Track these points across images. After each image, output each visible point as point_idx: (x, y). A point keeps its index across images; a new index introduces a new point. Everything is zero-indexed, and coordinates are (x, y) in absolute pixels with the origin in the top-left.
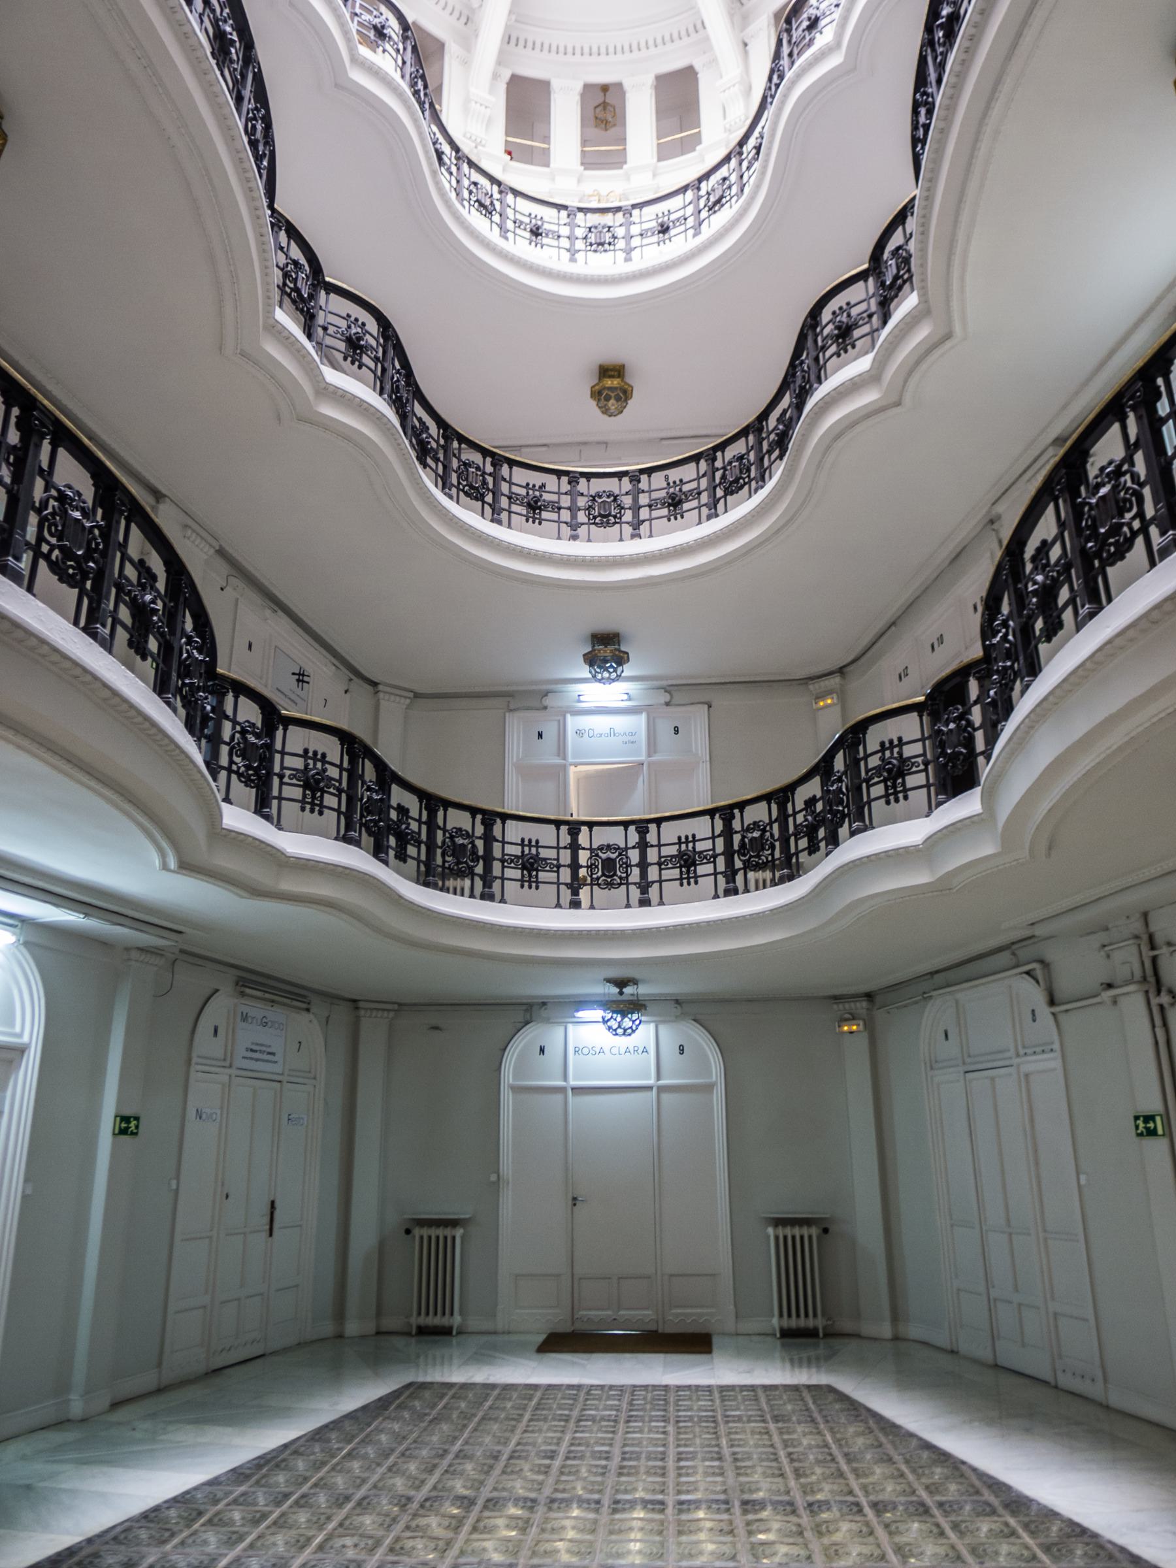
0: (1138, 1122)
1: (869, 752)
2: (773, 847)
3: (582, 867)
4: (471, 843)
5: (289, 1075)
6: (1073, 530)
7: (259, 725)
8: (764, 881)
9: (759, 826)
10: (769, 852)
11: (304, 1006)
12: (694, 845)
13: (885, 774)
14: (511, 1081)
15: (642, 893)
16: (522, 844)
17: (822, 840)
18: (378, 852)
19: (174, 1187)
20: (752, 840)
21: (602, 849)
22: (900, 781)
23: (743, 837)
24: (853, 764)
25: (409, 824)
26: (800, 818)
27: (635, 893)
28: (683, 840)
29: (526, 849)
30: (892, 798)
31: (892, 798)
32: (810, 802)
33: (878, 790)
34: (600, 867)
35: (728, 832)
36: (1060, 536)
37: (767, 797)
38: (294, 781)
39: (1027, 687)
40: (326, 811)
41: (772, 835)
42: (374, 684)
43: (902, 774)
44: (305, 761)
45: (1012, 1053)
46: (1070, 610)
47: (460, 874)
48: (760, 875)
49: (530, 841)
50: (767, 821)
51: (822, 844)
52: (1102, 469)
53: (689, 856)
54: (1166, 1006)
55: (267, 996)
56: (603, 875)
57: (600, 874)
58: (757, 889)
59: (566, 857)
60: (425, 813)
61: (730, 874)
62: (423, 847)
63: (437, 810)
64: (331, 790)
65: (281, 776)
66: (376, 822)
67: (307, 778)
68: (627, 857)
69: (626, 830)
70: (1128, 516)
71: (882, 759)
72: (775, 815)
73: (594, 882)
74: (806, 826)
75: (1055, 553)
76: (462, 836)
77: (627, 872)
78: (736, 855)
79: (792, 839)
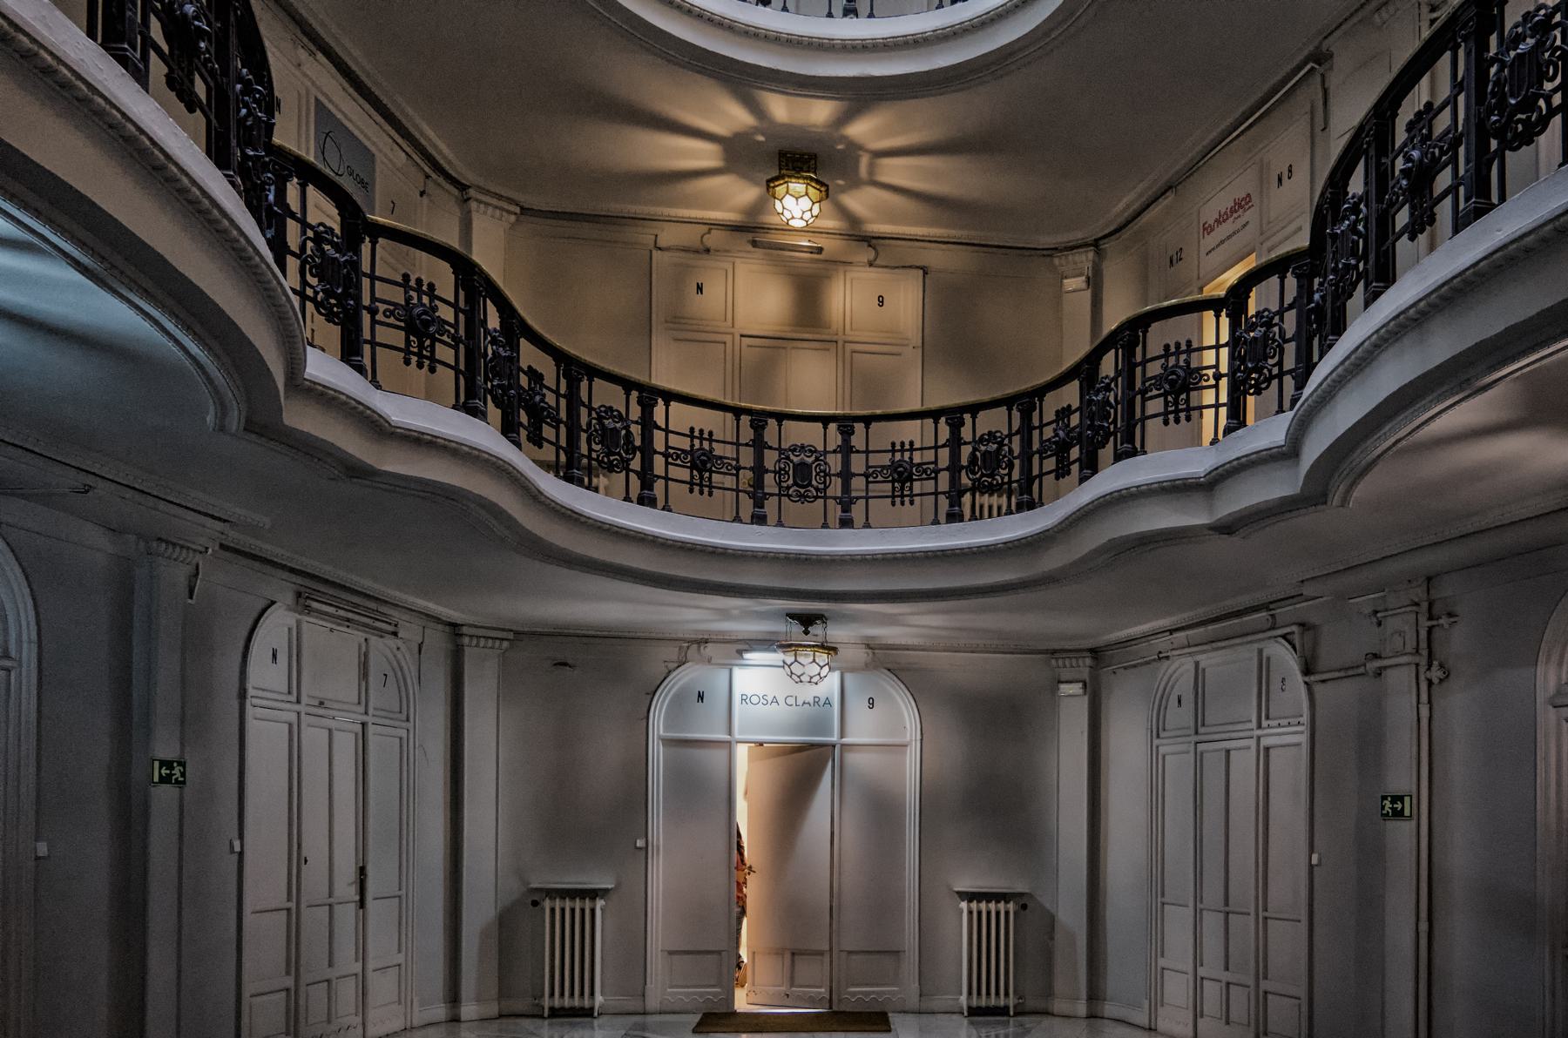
0: (1385, 802)
1: (1149, 356)
2: (1011, 466)
3: (767, 471)
4: (624, 428)
5: (374, 716)
6: (1473, 92)
7: (338, 231)
8: (999, 508)
9: (995, 438)
10: (1006, 471)
11: (391, 628)
12: (912, 454)
13: (1167, 387)
14: (661, 732)
15: (844, 511)
16: (691, 436)
17: (1074, 462)
18: (509, 429)
19: (237, 849)
20: (984, 454)
21: (795, 450)
22: (1183, 396)
23: (975, 449)
24: (1127, 370)
25: (544, 395)
26: (1048, 432)
27: (835, 511)
28: (898, 447)
29: (697, 442)
30: (1171, 417)
31: (1171, 417)
32: (1064, 413)
33: (1155, 406)
34: (791, 472)
35: (955, 442)
36: (1452, 101)
37: (1007, 402)
38: (392, 320)
39: (1376, 295)
40: (439, 368)
41: (1011, 451)
42: (462, 187)
43: (1186, 388)
44: (406, 292)
45: (1254, 724)
46: (1448, 201)
47: (610, 468)
48: (995, 500)
49: (701, 431)
50: (1006, 432)
51: (1075, 468)
52: (1527, 17)
53: (906, 469)
54: (1436, 681)
55: (341, 613)
56: (795, 483)
57: (791, 482)
58: (990, 516)
59: (747, 456)
60: (563, 382)
61: (955, 494)
62: (563, 429)
63: (581, 380)
64: (445, 338)
65: (373, 312)
66: (505, 389)
67: (411, 316)
68: (826, 463)
69: (825, 428)
70: (1271, 362)
71: (1165, 367)
72: (1016, 424)
73: (783, 493)
74: (1054, 443)
75: (1443, 122)
76: (612, 417)
77: (825, 482)
78: (963, 472)
79: (1036, 457)
